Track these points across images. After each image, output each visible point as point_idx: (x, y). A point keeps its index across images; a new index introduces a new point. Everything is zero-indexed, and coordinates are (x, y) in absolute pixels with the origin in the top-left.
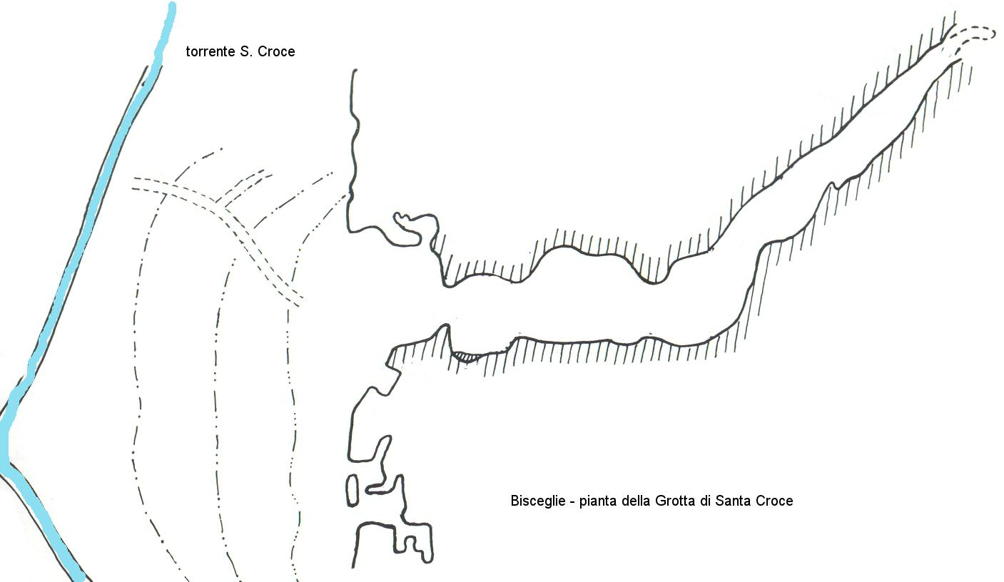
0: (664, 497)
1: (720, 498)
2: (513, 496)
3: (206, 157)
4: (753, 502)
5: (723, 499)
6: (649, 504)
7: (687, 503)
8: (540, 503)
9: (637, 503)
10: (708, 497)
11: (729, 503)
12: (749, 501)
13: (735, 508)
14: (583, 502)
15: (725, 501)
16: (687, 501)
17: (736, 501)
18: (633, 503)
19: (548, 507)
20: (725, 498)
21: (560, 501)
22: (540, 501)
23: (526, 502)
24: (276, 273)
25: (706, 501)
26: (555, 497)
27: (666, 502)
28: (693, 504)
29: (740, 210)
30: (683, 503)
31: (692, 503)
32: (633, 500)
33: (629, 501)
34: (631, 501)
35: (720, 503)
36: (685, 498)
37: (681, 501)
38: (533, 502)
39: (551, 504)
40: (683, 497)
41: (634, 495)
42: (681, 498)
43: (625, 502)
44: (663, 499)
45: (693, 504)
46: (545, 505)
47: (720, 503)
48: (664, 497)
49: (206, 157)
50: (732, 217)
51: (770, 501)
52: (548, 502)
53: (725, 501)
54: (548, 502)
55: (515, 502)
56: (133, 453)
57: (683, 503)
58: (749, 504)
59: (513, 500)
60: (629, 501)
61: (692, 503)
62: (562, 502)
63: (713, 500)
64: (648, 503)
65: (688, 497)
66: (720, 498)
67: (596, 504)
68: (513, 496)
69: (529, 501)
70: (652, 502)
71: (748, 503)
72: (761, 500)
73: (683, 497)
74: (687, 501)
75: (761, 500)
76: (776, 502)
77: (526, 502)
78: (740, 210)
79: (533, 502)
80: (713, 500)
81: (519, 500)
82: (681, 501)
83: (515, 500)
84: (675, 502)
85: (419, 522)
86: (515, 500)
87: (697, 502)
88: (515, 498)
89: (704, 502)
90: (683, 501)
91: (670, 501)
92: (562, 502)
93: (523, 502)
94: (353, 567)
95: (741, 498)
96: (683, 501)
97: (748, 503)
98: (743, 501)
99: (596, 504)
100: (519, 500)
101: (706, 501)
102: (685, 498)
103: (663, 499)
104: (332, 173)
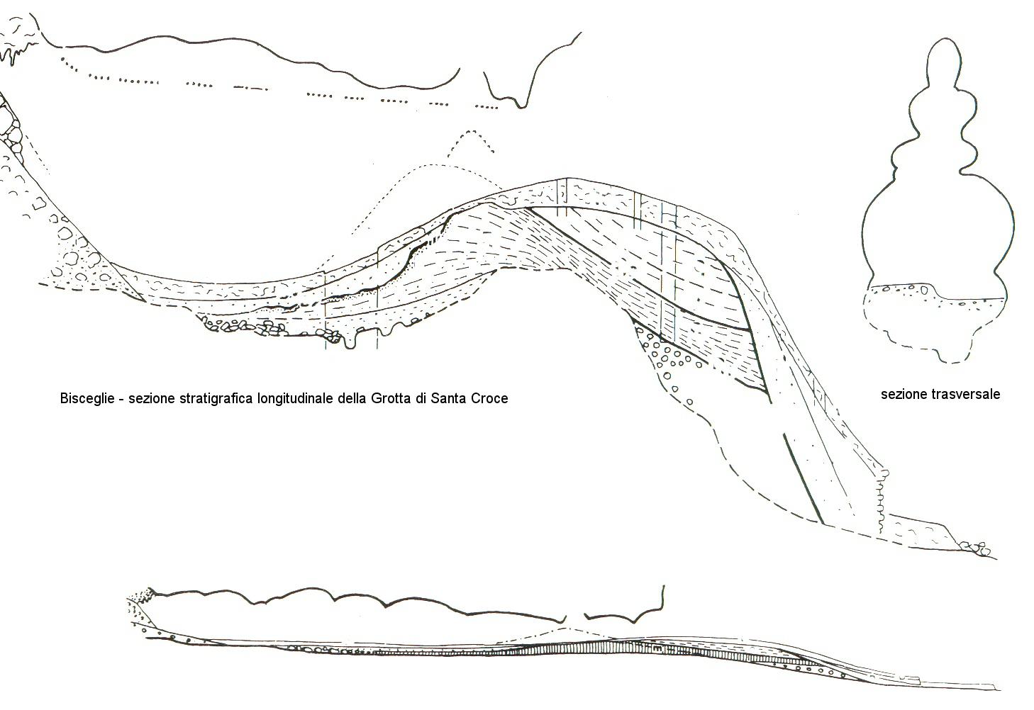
0: (380, 395)
1: (435, 395)
2: (62, 393)
3: (43, 36)
4: (468, 399)
5: (439, 397)
6: (364, 402)
7: (403, 400)
8: (90, 401)
9: (353, 400)
10: (424, 395)
11: (444, 400)
12: (409, 399)
13: (450, 406)
14: (132, 399)
15: (440, 399)
16: (403, 399)
17: (451, 398)
18: (349, 401)
19: (97, 404)
20: (440, 395)
21: (109, 399)
22: (89, 398)
23: (75, 399)
25: (422, 399)
26: (104, 395)
27: (382, 400)
28: (409, 402)
29: (769, 397)
30: (399, 400)
31: (408, 400)
32: (349, 398)
33: (345, 399)
34: (347, 399)
35: (435, 400)
36: (401, 396)
37: (396, 398)
38: (82, 399)
39: (217, 402)
41: (350, 393)
42: (397, 396)
43: (342, 399)
44: (379, 396)
45: (409, 402)
46: (94, 403)
47: (435, 400)
48: (380, 395)
49: (43, 36)
51: (485, 399)
52: (98, 399)
53: (440, 399)
54: (98, 399)
55: (64, 400)
57: (399, 400)
58: (464, 402)
59: (62, 398)
60: (345, 399)
61: (408, 400)
62: (111, 399)
63: (429, 398)
64: (363, 400)
65: (404, 395)
66: (435, 395)
67: (445, 402)
68: (62, 393)
69: (78, 399)
70: (368, 399)
71: (463, 400)
72: (476, 398)
74: (403, 399)
75: (476, 398)
76: (492, 399)
77: (75, 399)
78: (769, 397)
79: (82, 399)
80: (429, 398)
81: (68, 397)
82: (396, 398)
83: (65, 398)
84: (391, 399)
86: (65, 398)
87: (413, 399)
88: (64, 395)
89: (420, 399)
90: (399, 398)
91: (386, 399)
92: (111, 399)
93: (72, 400)
95: (456, 396)
96: (399, 398)
97: (463, 400)
98: (458, 399)
99: (445, 402)
100: (68, 397)
101: (422, 399)
102: (401, 396)
103: (379, 396)
104: (188, 84)
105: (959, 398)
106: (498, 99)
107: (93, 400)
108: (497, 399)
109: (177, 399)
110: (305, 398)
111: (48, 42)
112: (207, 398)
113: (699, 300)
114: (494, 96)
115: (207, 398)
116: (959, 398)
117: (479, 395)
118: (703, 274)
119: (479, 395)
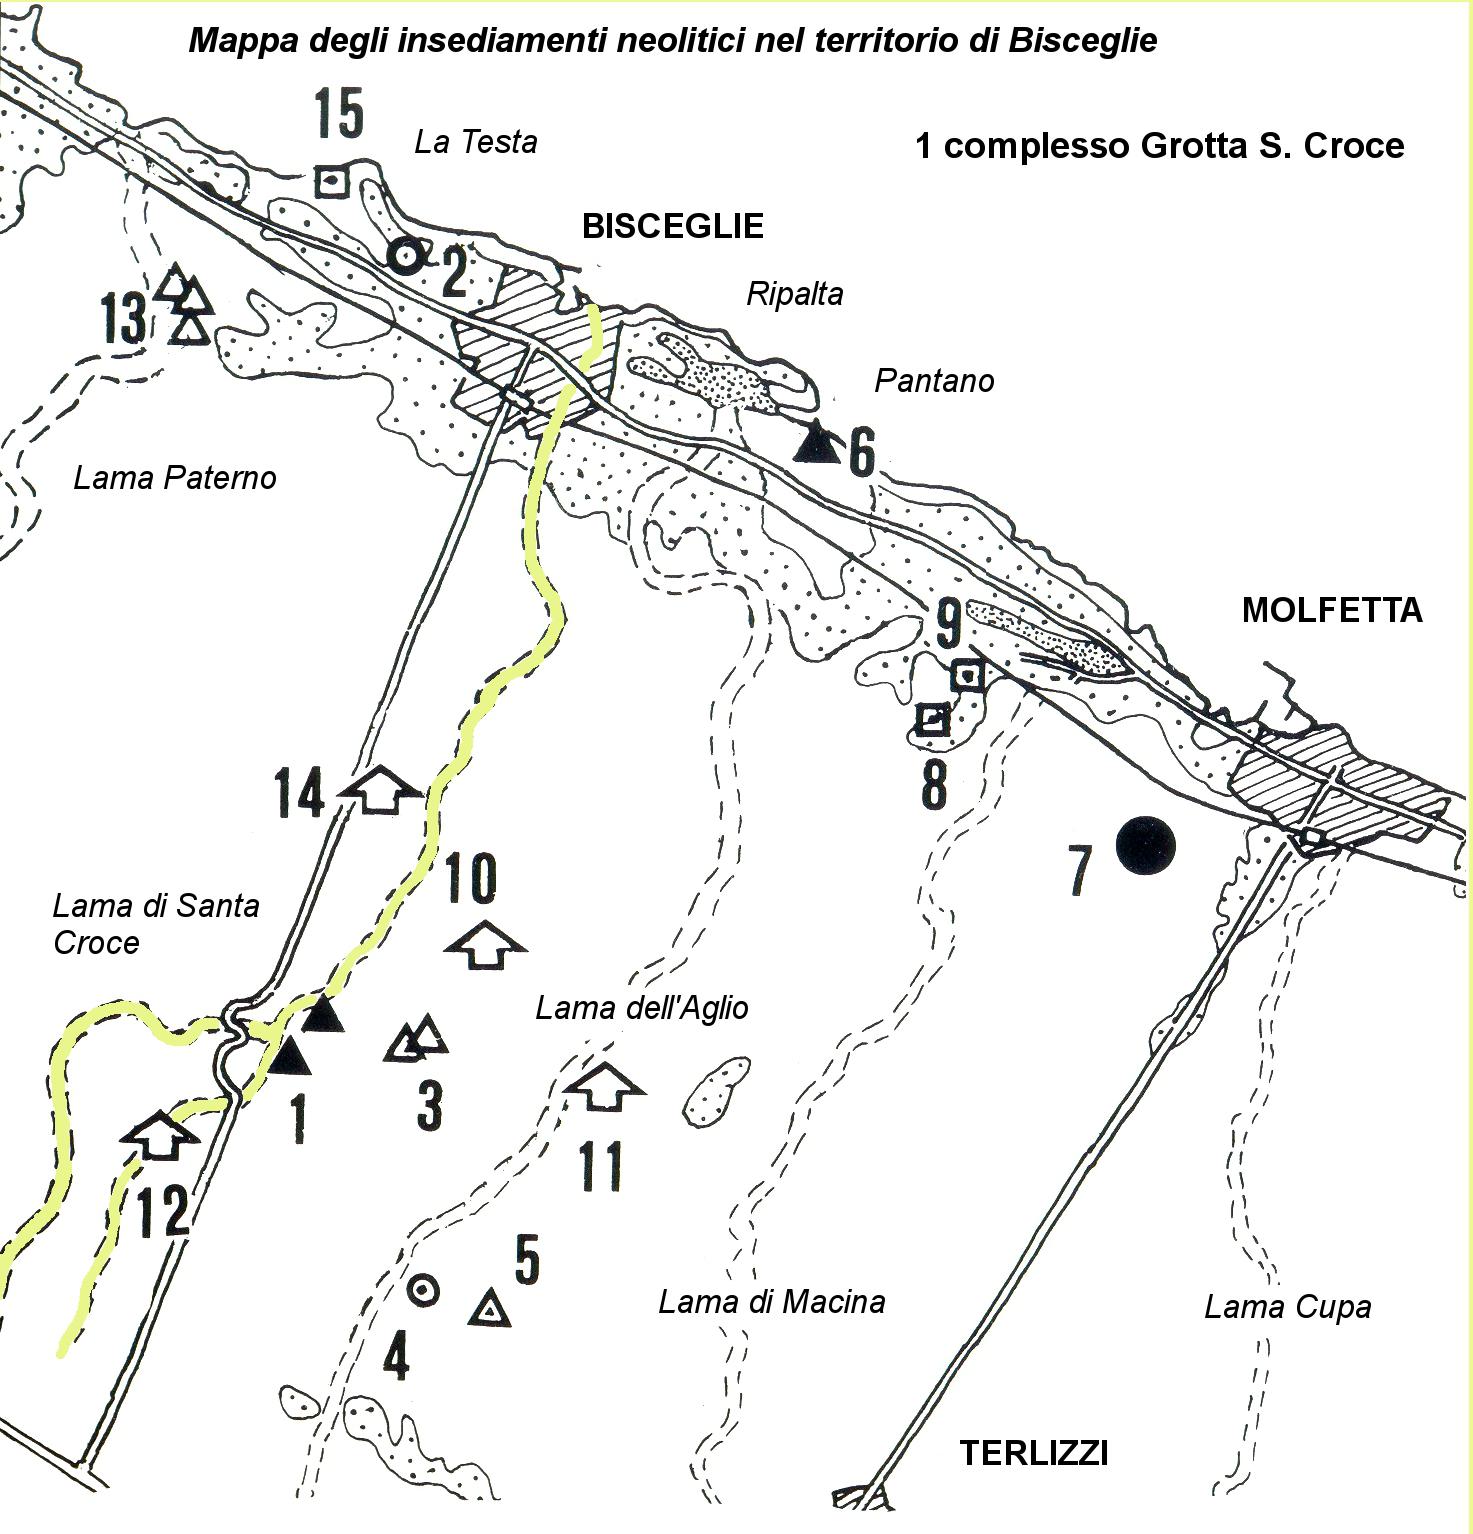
11: (209, 909)
16: (1228, 146)
20: (200, 899)
22: (1089, 42)
24: (1253, 1230)
25: (985, 41)
26: (728, 999)
34: (648, 1009)
35: (186, 910)
36: (824, 288)
38: (1072, 42)
40: (1216, 136)
47: (186, 910)
50: (498, 320)
56: (599, 483)
66: (187, 899)
73: (1216, 136)
80: (173, 903)
82: (1217, 146)
85: (916, 665)
88: (594, 220)
90: (1215, 146)
94: (1077, 891)
96: (1215, 146)
100: (1034, 39)
101: (985, 41)
102: (824, 288)
105: (794, 1311)
106: (391, 383)
107: (348, 45)
108: (115, 945)
109: (303, 44)
110: (888, 40)
111: (1095, 716)
112: (707, 41)
113: (290, 338)
114: (392, 387)
115: (707, 41)
116: (794, 1311)
117: (1323, 137)
118: (599, 483)
119: (1323, 137)
